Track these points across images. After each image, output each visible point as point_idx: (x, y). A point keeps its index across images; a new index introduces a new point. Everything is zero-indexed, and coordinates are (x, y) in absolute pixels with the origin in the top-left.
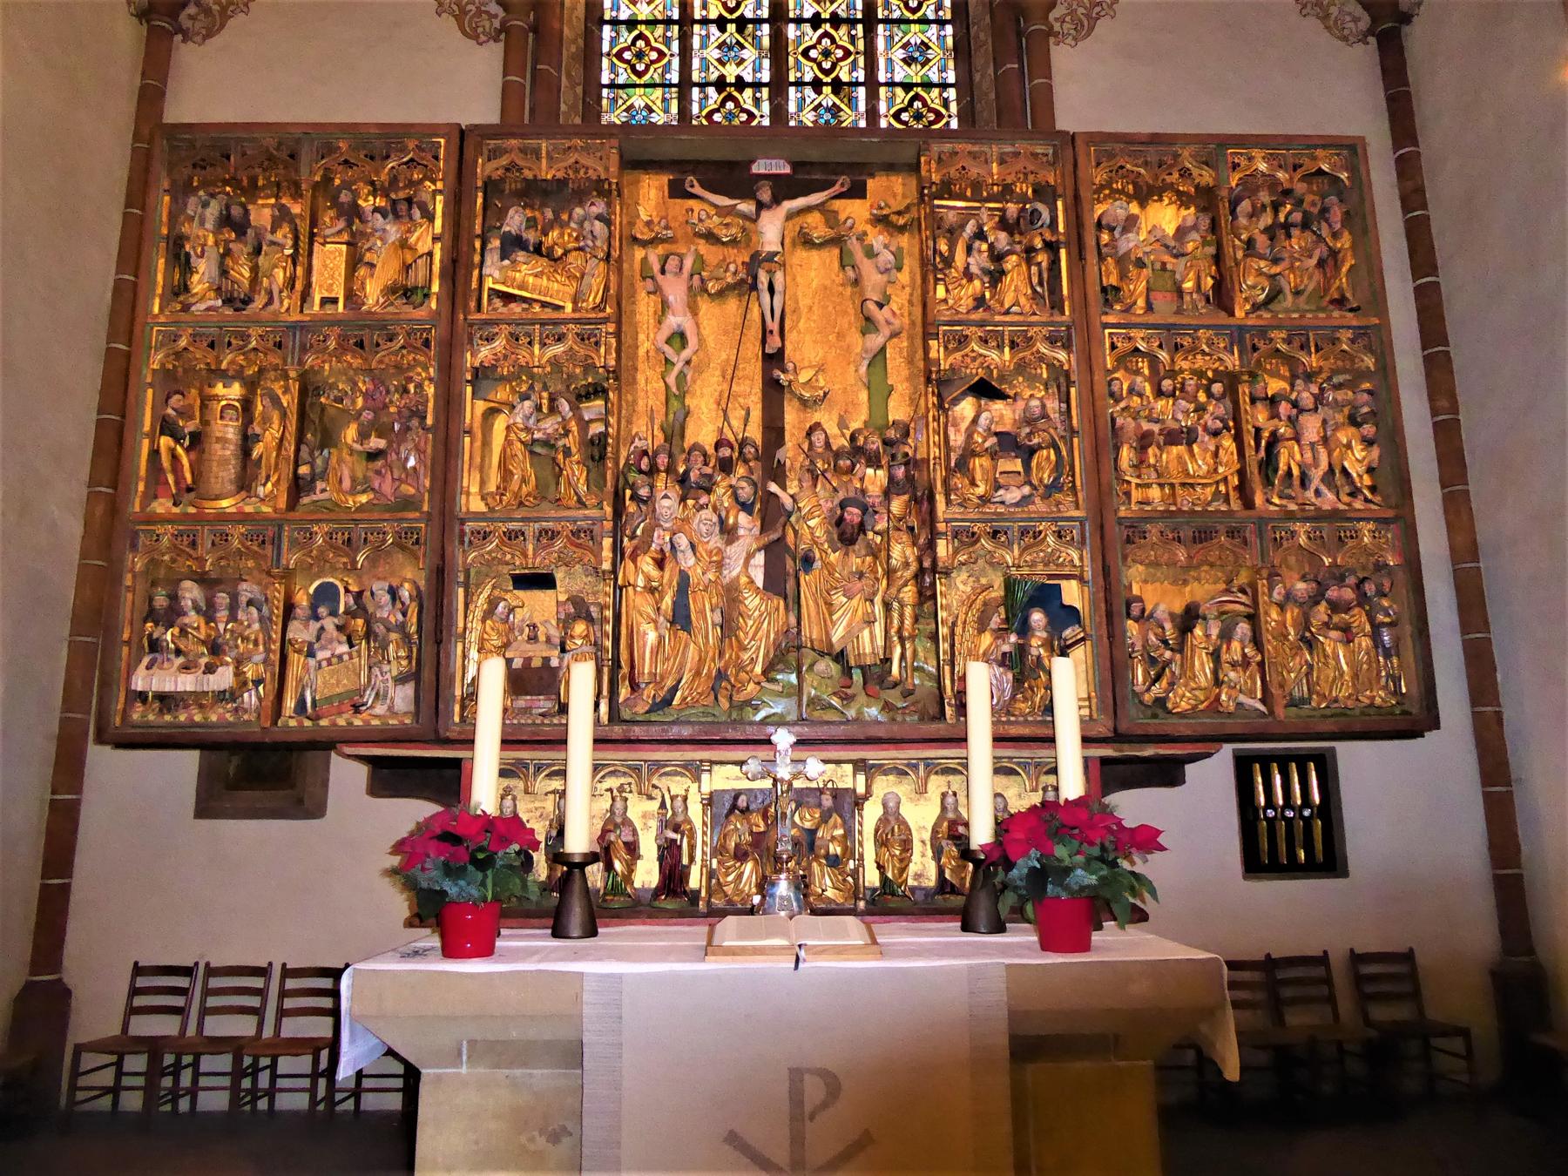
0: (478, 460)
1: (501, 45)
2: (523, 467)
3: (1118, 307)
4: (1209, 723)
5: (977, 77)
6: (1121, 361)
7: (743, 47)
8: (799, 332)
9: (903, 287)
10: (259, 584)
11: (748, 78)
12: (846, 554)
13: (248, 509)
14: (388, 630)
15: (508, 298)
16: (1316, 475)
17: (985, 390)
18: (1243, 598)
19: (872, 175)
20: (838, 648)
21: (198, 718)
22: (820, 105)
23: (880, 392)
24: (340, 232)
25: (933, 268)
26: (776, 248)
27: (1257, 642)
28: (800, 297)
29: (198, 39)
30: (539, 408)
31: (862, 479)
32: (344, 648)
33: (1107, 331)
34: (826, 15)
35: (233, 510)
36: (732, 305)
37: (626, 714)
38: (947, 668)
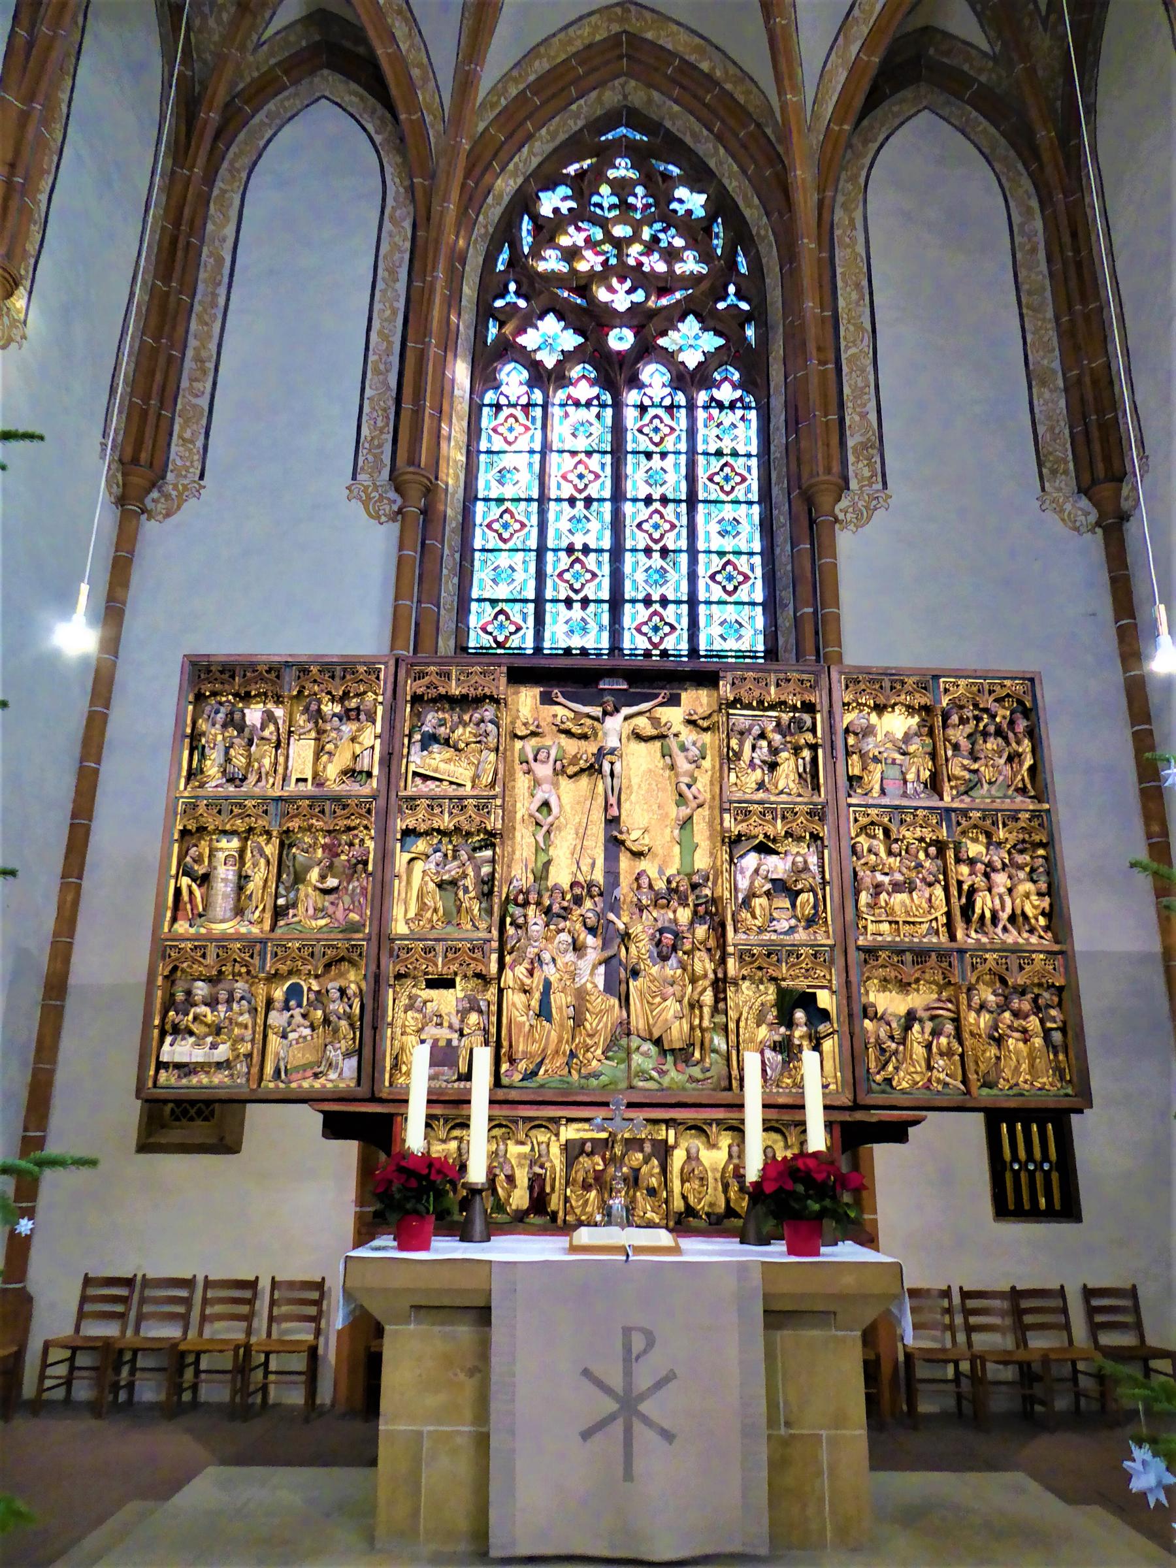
0: (403, 895)
1: (397, 525)
2: (435, 899)
3: (859, 791)
4: (922, 1097)
6: (863, 829)
7: (588, 520)
10: (247, 982)
11: (593, 546)
12: (663, 967)
13: (243, 930)
14: (339, 1018)
15: (426, 778)
16: (1004, 916)
17: (763, 849)
18: (950, 1006)
19: (686, 690)
20: (656, 1035)
22: (650, 567)
23: (688, 848)
25: (730, 758)
27: (959, 1037)
29: (160, 517)
30: (446, 855)
31: (675, 912)
32: (307, 1032)
33: (852, 809)
34: (656, 496)
35: (232, 931)
36: (584, 781)
37: (505, 1081)
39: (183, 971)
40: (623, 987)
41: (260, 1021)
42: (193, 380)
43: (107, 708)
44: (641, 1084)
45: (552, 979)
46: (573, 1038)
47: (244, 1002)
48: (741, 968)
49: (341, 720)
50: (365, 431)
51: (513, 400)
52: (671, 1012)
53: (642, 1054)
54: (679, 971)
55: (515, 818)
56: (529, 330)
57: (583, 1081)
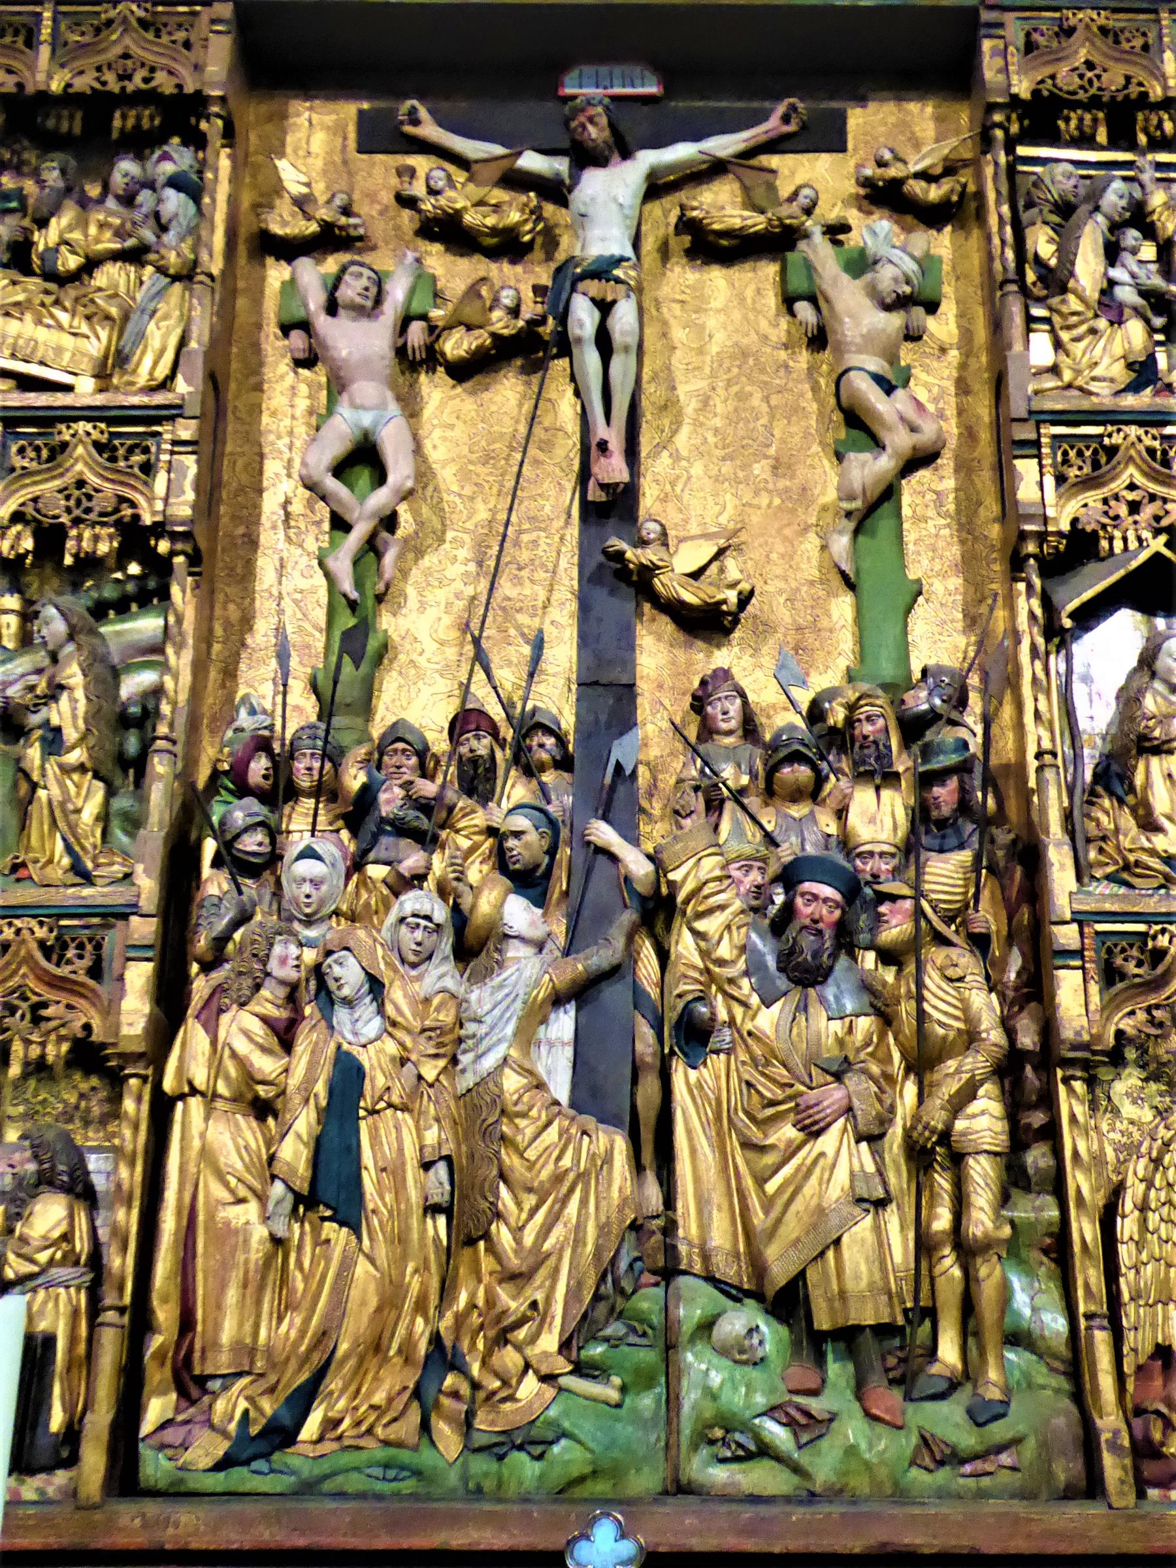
5: (1005, 209)
8: (676, 457)
9: (943, 350)
12: (803, 1007)
19: (862, 100)
20: (780, 1272)
26: (619, 246)
28: (679, 376)
31: (841, 814)
38: (1102, 1339)
40: (649, 1087)
44: (720, 1474)
45: (366, 1058)
46: (447, 1290)
48: (1109, 1007)
52: (841, 1177)
53: (723, 1351)
54: (865, 1024)
55: (256, 508)
57: (481, 1465)
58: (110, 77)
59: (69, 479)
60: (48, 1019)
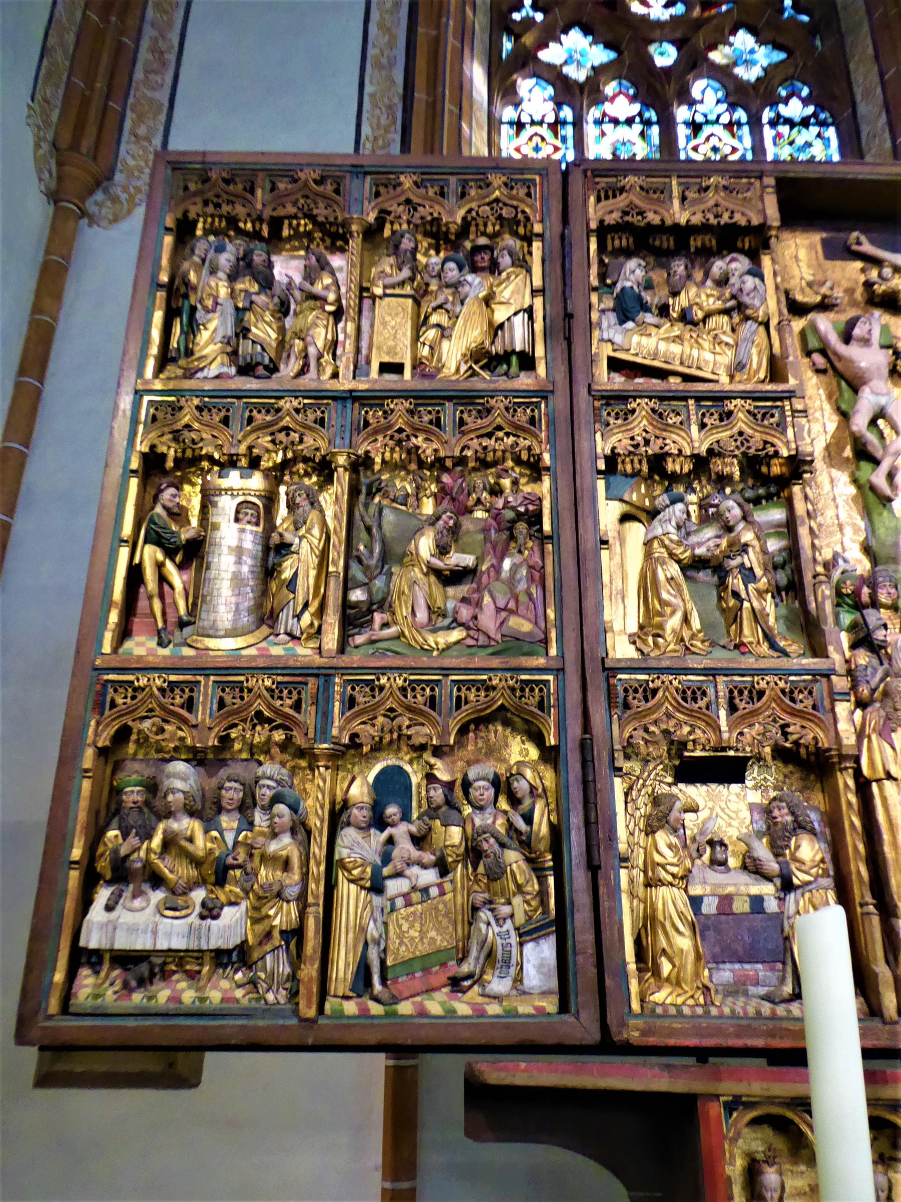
10: (283, 764)
13: (276, 651)
14: (503, 845)
21: (189, 996)
24: (402, 284)
32: (429, 876)
39: (144, 740)
41: (318, 850)
42: (147, 72)
43: (27, 447)
47: (281, 808)
49: (461, 268)
50: (366, 130)
51: (537, 118)
56: (551, 44)
58: (711, 216)
59: (735, 430)
60: (792, 734)
